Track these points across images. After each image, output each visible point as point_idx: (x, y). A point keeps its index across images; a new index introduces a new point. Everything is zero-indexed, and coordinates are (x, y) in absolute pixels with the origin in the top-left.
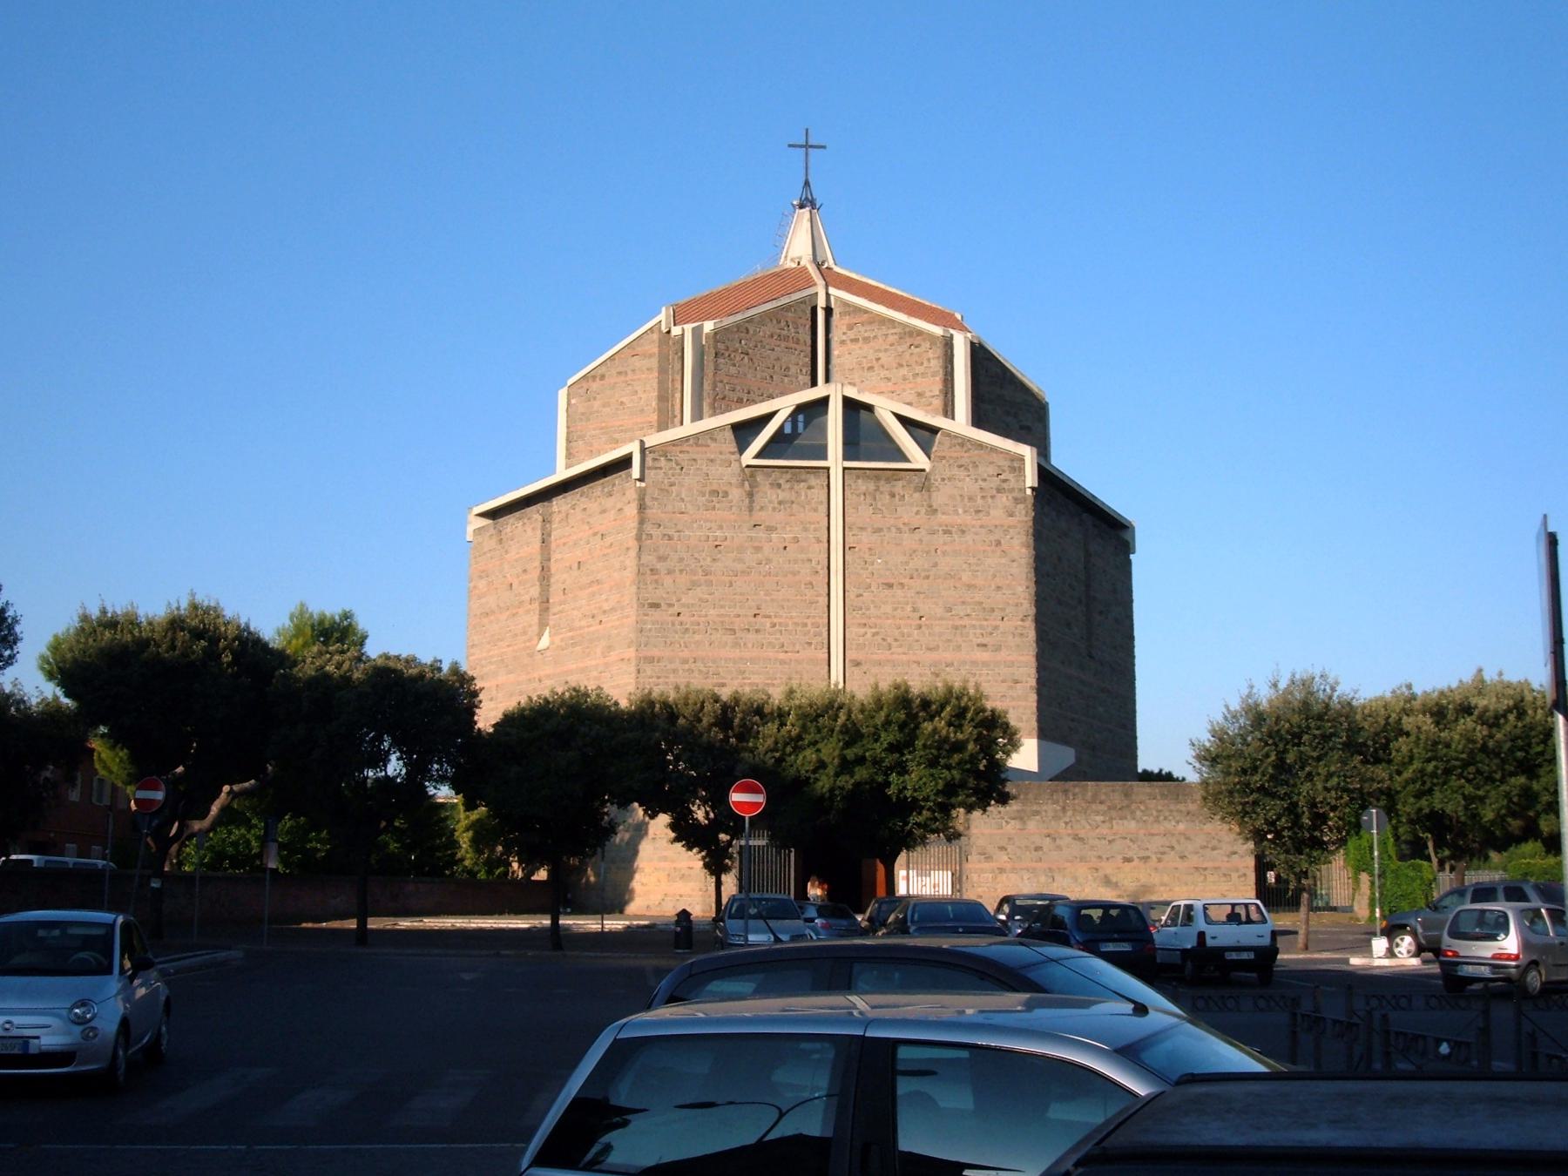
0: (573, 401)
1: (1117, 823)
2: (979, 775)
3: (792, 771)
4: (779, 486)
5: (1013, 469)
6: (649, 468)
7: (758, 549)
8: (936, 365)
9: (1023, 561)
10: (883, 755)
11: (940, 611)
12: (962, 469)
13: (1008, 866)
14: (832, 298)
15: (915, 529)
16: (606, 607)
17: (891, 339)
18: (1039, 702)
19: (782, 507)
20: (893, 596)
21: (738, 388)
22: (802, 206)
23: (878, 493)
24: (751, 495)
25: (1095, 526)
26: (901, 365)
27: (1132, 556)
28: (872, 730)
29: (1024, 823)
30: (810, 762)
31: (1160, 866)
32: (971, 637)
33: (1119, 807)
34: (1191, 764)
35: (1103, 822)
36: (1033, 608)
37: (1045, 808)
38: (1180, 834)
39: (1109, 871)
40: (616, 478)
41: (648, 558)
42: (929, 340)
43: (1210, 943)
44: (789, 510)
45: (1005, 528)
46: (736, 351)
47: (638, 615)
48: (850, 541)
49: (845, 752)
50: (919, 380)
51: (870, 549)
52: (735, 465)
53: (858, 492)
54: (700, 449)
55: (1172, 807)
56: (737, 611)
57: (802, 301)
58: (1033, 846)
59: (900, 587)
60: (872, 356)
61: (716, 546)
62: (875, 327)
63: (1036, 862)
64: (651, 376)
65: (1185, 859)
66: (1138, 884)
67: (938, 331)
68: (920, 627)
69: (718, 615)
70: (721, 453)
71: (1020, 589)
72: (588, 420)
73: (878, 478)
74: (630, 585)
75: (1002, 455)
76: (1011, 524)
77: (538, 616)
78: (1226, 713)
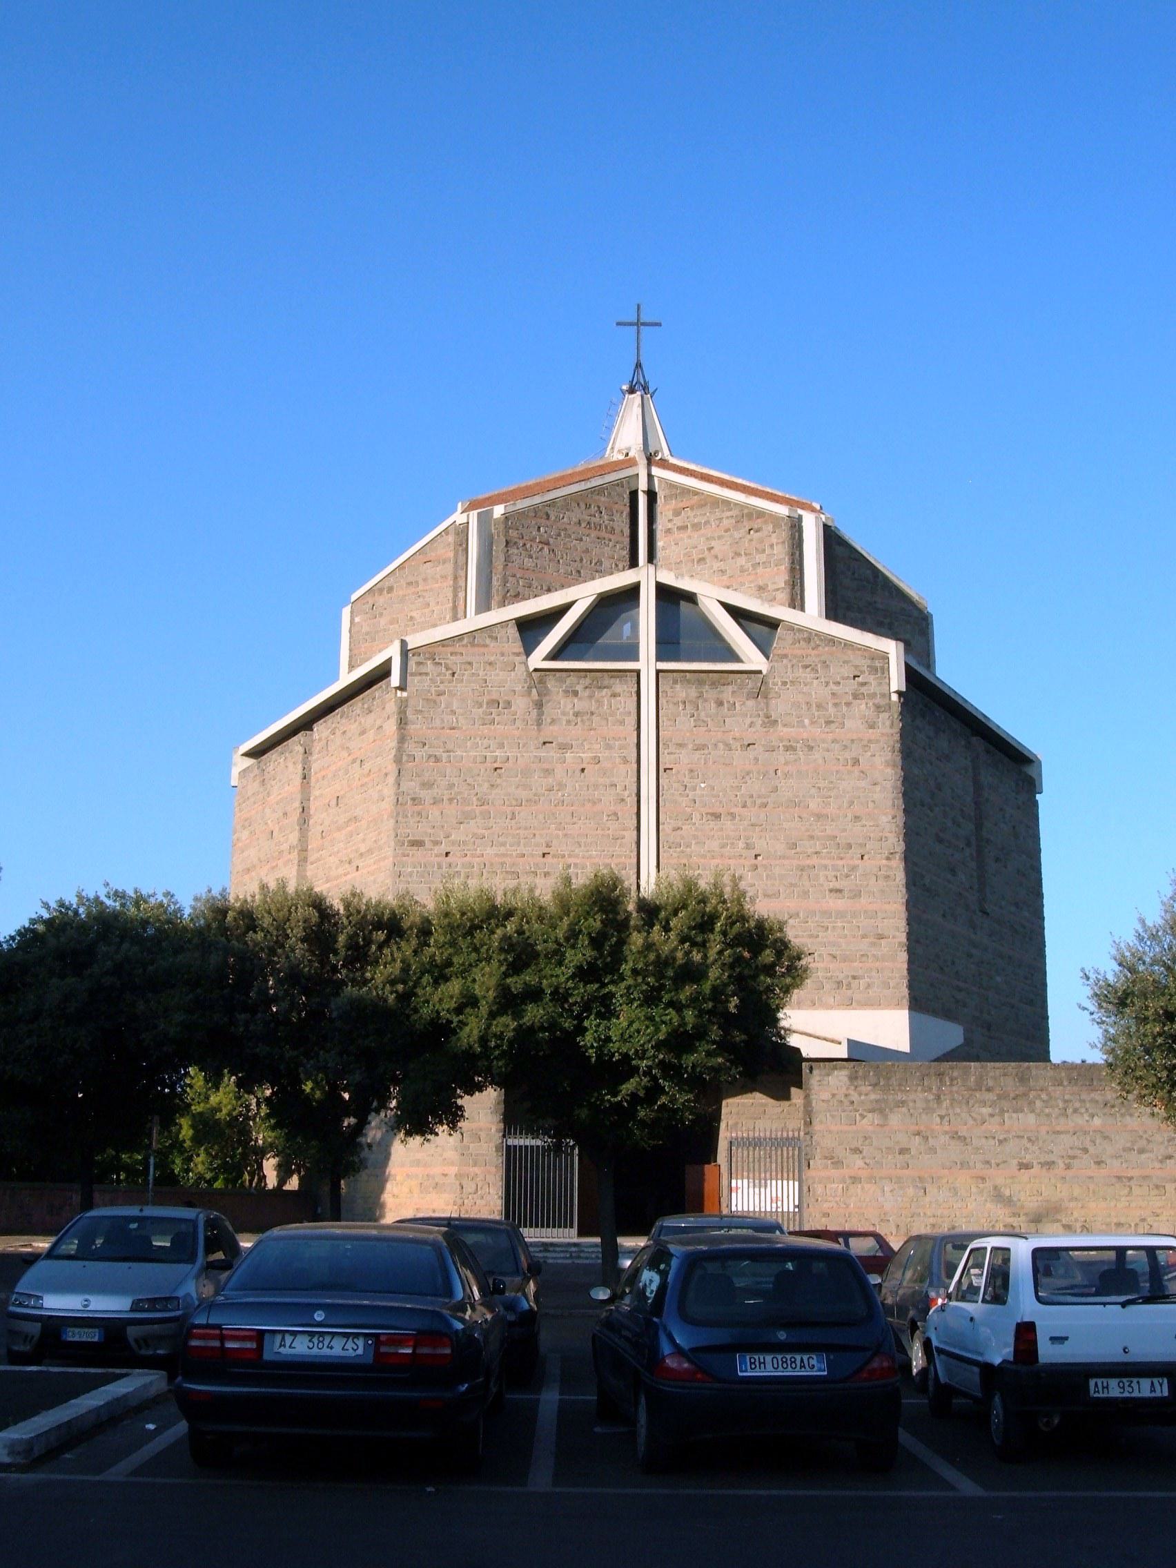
0: (357, 620)
1: (1010, 1118)
2: (728, 1021)
3: (425, 1011)
4: (576, 693)
5: (873, 670)
6: (412, 674)
7: (548, 772)
8: (781, 551)
9: (889, 785)
10: (570, 984)
11: (780, 848)
12: (808, 670)
13: (864, 1174)
14: (656, 479)
15: (749, 745)
16: (363, 849)
17: (726, 522)
18: (910, 962)
19: (579, 719)
20: (721, 830)
21: (535, 583)
22: (632, 391)
23: (700, 701)
24: (539, 705)
25: (988, 752)
26: (738, 554)
27: (1038, 796)
28: (551, 946)
29: (886, 1117)
30: (452, 997)
31: (1070, 1173)
32: (822, 879)
33: (1012, 1095)
34: (1084, 1009)
35: (992, 1115)
36: (902, 843)
37: (912, 1096)
38: (1095, 1131)
39: (1000, 1181)
40: (376, 690)
41: (409, 785)
42: (772, 522)
43: (1047, 1353)
44: (587, 724)
45: (865, 743)
46: (533, 540)
47: (395, 857)
48: (666, 761)
49: (509, 980)
50: (760, 570)
51: (692, 771)
52: (520, 669)
53: (675, 700)
54: (476, 649)
55: (1084, 1096)
56: (521, 850)
57: (619, 483)
58: (897, 1148)
59: (730, 818)
60: (703, 546)
61: (496, 769)
62: (708, 509)
63: (902, 1168)
64: (445, 584)
65: (1103, 1165)
66: (1040, 1199)
67: (782, 510)
68: (756, 867)
69: (497, 855)
70: (503, 655)
71: (885, 819)
72: (374, 640)
73: (701, 683)
74: (388, 820)
75: (860, 653)
76: (873, 737)
77: (297, 867)
78: (1141, 931)
